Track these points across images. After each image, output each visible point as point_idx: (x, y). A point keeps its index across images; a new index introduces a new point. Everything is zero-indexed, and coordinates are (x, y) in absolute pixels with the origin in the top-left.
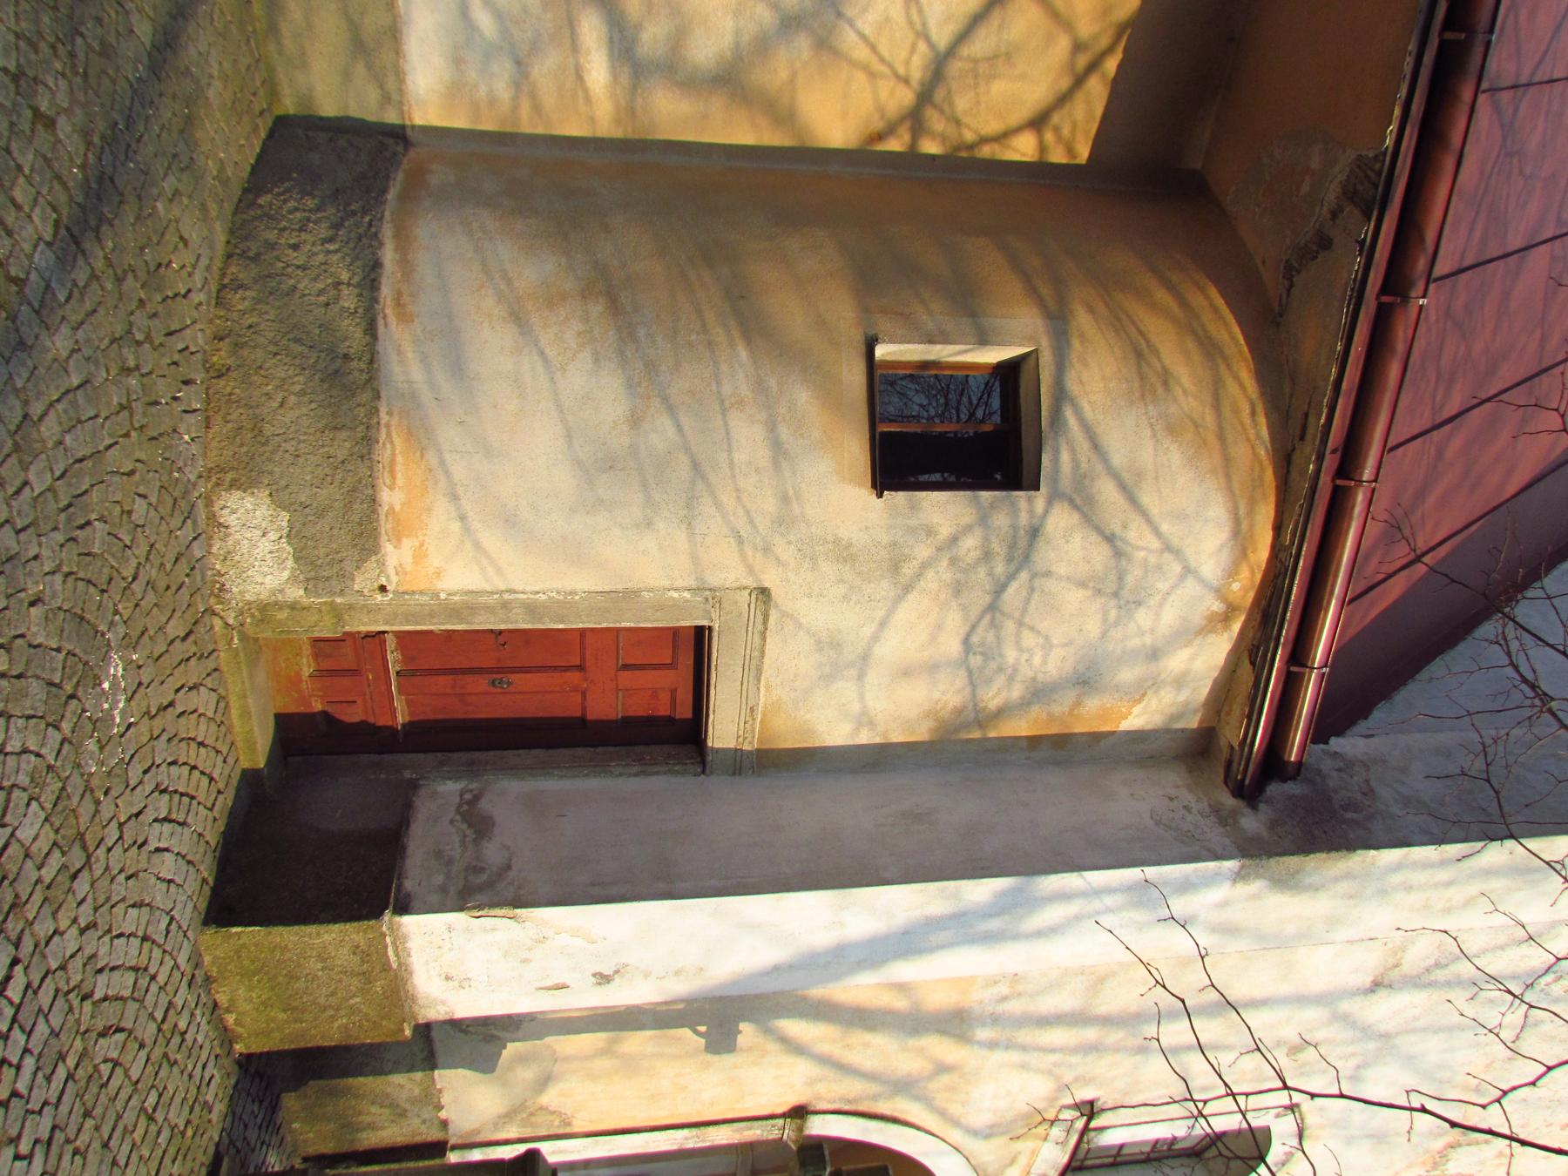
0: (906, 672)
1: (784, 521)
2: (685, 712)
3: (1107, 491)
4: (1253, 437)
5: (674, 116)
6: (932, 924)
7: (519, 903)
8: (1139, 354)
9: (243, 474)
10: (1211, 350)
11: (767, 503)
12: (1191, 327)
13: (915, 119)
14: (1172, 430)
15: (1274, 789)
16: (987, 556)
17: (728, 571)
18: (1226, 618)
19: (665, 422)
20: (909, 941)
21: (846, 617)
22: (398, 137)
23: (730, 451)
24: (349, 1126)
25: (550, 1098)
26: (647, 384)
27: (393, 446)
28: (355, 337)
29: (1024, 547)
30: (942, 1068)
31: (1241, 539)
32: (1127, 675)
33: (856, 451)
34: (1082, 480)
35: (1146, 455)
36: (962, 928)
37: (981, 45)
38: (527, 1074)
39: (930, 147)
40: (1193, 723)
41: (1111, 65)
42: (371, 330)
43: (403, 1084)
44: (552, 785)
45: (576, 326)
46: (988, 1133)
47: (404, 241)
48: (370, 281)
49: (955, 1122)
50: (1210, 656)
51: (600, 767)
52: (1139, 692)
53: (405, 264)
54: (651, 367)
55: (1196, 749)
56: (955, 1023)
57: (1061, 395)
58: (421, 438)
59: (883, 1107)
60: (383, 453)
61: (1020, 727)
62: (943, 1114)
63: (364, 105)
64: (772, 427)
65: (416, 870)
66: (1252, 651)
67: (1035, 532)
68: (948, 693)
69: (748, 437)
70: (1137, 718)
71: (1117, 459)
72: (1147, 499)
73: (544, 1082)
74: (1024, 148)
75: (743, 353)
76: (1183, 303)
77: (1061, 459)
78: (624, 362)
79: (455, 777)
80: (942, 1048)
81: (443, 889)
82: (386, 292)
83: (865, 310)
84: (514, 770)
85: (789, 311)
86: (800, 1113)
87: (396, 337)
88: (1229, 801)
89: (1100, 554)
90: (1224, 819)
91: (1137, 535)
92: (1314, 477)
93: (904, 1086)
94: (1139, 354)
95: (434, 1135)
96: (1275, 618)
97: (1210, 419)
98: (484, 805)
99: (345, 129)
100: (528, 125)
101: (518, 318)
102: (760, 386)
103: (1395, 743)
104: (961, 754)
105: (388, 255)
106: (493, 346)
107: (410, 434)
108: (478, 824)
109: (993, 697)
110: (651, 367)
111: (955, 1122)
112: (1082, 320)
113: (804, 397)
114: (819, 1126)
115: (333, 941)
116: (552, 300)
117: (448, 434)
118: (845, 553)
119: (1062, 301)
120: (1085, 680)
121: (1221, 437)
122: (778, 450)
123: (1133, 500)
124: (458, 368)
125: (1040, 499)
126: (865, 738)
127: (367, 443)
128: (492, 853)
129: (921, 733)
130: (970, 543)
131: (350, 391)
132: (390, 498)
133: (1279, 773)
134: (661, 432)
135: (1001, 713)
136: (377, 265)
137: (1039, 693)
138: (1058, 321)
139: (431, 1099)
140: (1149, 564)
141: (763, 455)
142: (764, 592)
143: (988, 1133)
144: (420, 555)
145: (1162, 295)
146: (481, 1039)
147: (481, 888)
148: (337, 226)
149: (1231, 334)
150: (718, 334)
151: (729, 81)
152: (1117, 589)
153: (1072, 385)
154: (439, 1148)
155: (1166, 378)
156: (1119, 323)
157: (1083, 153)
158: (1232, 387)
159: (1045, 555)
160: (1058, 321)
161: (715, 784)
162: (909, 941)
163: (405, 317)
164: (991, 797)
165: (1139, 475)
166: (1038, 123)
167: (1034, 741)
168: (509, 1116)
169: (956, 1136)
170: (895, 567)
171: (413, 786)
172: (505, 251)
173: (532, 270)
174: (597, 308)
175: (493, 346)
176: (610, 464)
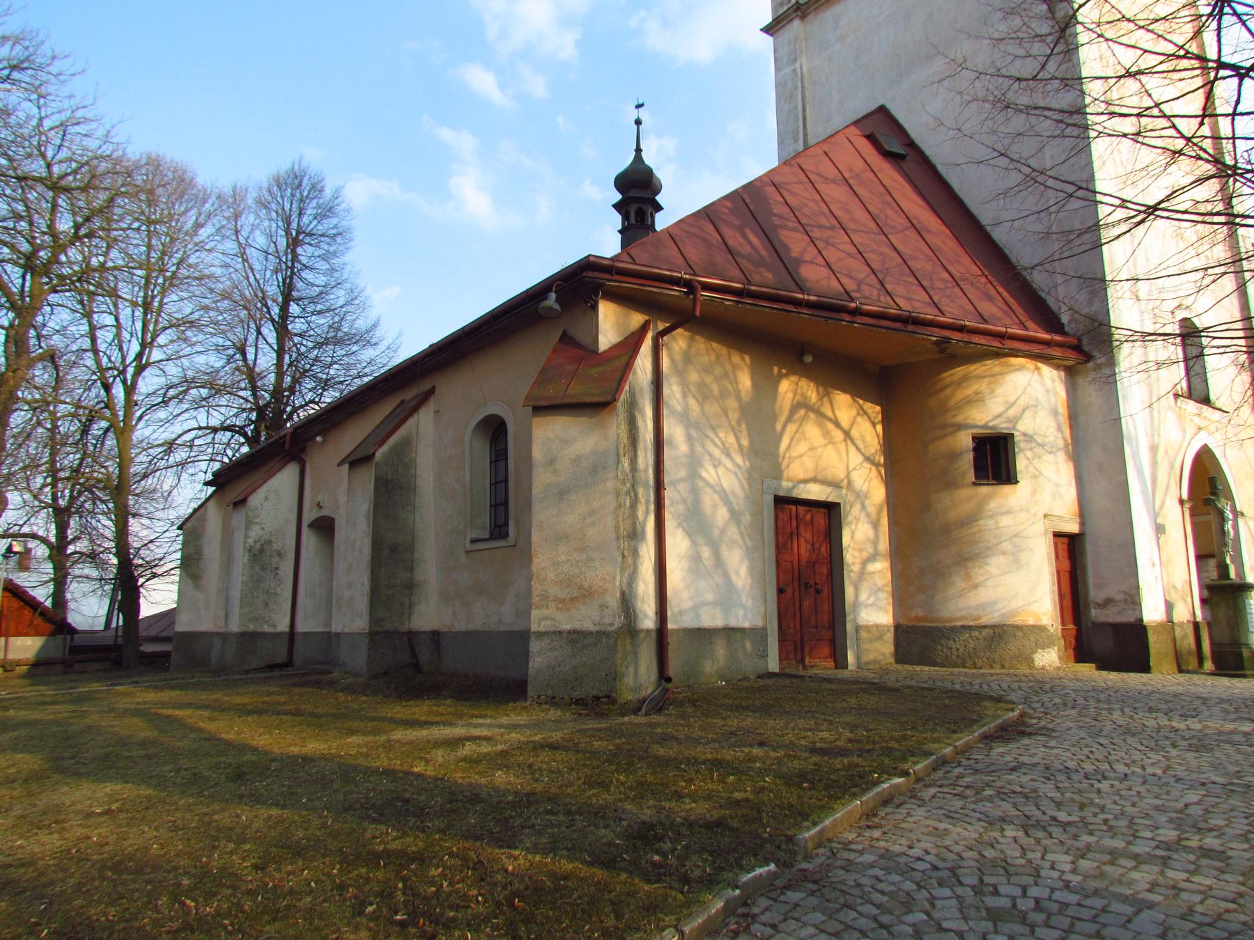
0: (1058, 471)
1: (1027, 510)
2: (1065, 540)
3: (1011, 412)
4: (991, 365)
5: (884, 545)
6: (1135, 464)
7: (1138, 588)
8: (969, 402)
9: (1029, 661)
10: (965, 378)
11: (1024, 514)
12: (959, 384)
13: (877, 465)
14: (992, 392)
15: (1086, 348)
16: (1031, 449)
17: (1039, 527)
18: (1037, 369)
19: (1004, 544)
20: (1140, 472)
21: (1044, 493)
22: (897, 627)
23: (122, 517)
24: (1190, 652)
25: (1179, 586)
26: (991, 550)
27: (1018, 620)
28: (985, 632)
29: (1028, 437)
30: (1166, 453)
31: (1021, 368)
32: (1053, 399)
33: (1006, 489)
34: (1009, 421)
35: (1000, 400)
36: (1135, 455)
37: (861, 446)
38: (1173, 593)
39: (882, 461)
40: (1063, 373)
41: (861, 402)
42: (985, 627)
43: (1178, 632)
44: (1091, 581)
45: (977, 570)
46: (1184, 432)
47: (949, 620)
48: (970, 628)
49: (1181, 445)
50: (1046, 370)
51: (1084, 567)
52: (1056, 394)
53: (960, 619)
54: (988, 548)
55: (1071, 372)
56: (1154, 449)
57: (985, 427)
58: (1014, 613)
59: (1178, 472)
60: (1019, 623)
61: (1067, 432)
62: (1179, 450)
63: (890, 637)
64: (1002, 514)
65: (1128, 618)
66: (1046, 359)
67: (1025, 435)
68: (1061, 457)
69: (1005, 521)
70: (1062, 393)
71: (1002, 409)
72: (1012, 399)
73: (1175, 587)
74: (879, 428)
75: (981, 522)
76: (951, 384)
77: (1003, 426)
78: (988, 556)
79: (1089, 611)
80: (1161, 452)
81: (1134, 610)
82: (971, 623)
83: (963, 486)
84: (1086, 593)
85: (965, 509)
86: (1181, 502)
87: (985, 620)
88: (1090, 365)
89: (1028, 414)
90: (1098, 367)
91: (1022, 402)
92: (1002, 346)
93: (1172, 466)
94: (969, 402)
95: (1191, 625)
96: (1039, 353)
97: (987, 380)
98: (1100, 601)
99: (897, 644)
100: (889, 589)
101: (976, 586)
102: (991, 517)
103: (1064, 297)
104: (1077, 452)
105: (959, 624)
106: (984, 595)
107: (1014, 616)
108: (1108, 602)
109: (1061, 443)
110: (988, 548)
111: (1181, 445)
112: (959, 419)
113: (993, 505)
114: (1185, 496)
115: (1152, 639)
116: (968, 577)
117: (1013, 605)
118: (1034, 492)
119: (954, 425)
120: (1055, 413)
121: (992, 376)
122: (1008, 512)
123: (1012, 405)
124: (994, 603)
125: (1016, 433)
126: (1073, 483)
127: (1017, 627)
128: (1119, 597)
129: (1071, 465)
130: (1029, 454)
131: (1005, 632)
132: (1031, 622)
133: (1082, 346)
134: (1006, 546)
135: (1065, 440)
136: (963, 627)
137: (1059, 429)
138: (959, 427)
139: (1181, 625)
140: (1023, 396)
141: (1011, 516)
142: (1045, 516)
143: (1184, 432)
144: (1044, 614)
145: (948, 391)
146: (1169, 607)
147: (1133, 598)
148: (949, 639)
149: (959, 371)
150: (975, 529)
151: (875, 525)
152: (1033, 407)
153: (981, 423)
154: (1196, 625)
155: (977, 393)
156: (960, 407)
157: (878, 408)
158: (978, 372)
159: (1030, 432)
160: (959, 427)
161: (1088, 530)
162: (1140, 472)
163: (979, 618)
164: (1096, 445)
165: (1006, 402)
166: (874, 425)
167: (1071, 427)
168: (1185, 600)
169: (1185, 444)
170: (1036, 477)
171: (1094, 624)
172: (952, 591)
173: (959, 583)
174: (970, 564)
175: (984, 595)
176: (1017, 560)
